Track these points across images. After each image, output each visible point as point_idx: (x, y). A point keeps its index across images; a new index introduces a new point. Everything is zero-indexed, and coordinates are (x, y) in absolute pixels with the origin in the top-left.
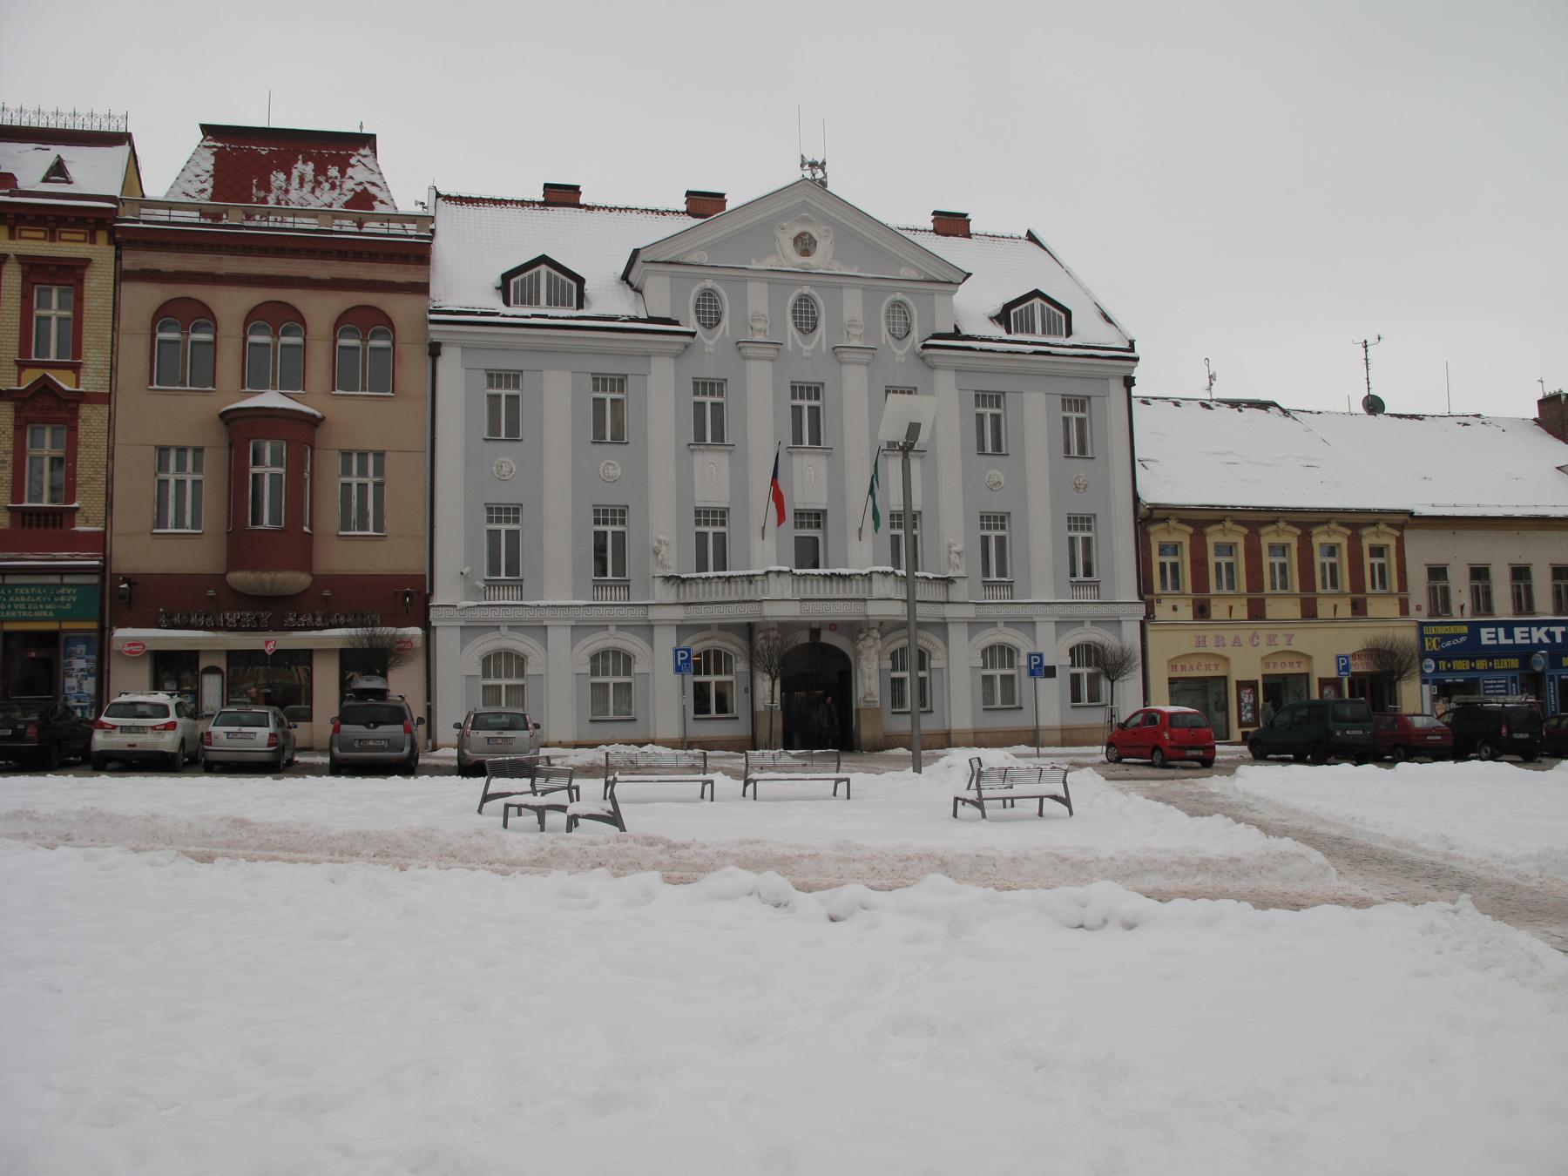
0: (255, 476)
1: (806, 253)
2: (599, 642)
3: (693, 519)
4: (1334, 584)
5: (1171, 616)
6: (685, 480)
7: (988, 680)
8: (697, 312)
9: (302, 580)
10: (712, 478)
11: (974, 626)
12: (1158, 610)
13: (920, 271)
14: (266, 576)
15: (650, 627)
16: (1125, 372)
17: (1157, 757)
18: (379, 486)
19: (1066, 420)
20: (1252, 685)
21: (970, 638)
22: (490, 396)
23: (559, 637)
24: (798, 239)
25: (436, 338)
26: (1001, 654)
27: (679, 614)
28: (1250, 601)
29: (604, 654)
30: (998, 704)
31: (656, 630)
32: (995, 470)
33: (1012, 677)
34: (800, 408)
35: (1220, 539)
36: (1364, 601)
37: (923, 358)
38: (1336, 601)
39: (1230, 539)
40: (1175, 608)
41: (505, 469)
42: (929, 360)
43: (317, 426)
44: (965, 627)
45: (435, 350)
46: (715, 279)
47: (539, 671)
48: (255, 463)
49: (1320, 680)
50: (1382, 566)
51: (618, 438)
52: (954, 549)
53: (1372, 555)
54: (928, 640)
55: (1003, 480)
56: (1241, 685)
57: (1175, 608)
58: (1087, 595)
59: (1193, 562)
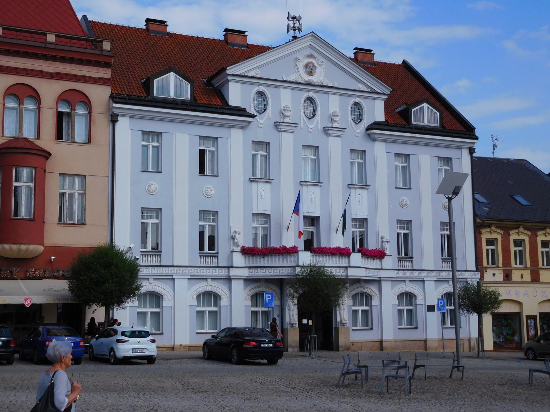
0: (16, 187)
1: (311, 74)
2: (202, 287)
3: (198, 217)
4: (521, 263)
5: (492, 279)
6: (248, 200)
7: (400, 311)
8: (254, 104)
9: (41, 248)
10: (263, 198)
11: (394, 281)
12: (486, 276)
13: (368, 87)
14: (24, 247)
15: (229, 280)
16: (470, 146)
17: (531, 355)
18: (82, 194)
19: (254, 156)
20: (534, 318)
21: (392, 289)
22: (143, 146)
23: (181, 284)
24: (307, 66)
25: (116, 111)
26: (408, 297)
27: (246, 273)
28: (532, 271)
29: (204, 294)
30: (360, 327)
31: (234, 282)
32: (405, 197)
33: (216, 312)
34: (147, 146)
35: (516, 237)
36: (510, 271)
37: (369, 135)
38: (494, 271)
39: (522, 237)
40: (494, 275)
41: (153, 188)
42: (372, 136)
43: (47, 158)
44: (242, 281)
45: (114, 119)
46: (264, 85)
47: (171, 304)
48: (16, 180)
49: (527, 316)
50: (520, 252)
51: (158, 170)
52: (384, 240)
53: (487, 245)
54: (372, 289)
55: (408, 203)
56: (528, 317)
57: (494, 275)
58: (406, 265)
59: (503, 250)
